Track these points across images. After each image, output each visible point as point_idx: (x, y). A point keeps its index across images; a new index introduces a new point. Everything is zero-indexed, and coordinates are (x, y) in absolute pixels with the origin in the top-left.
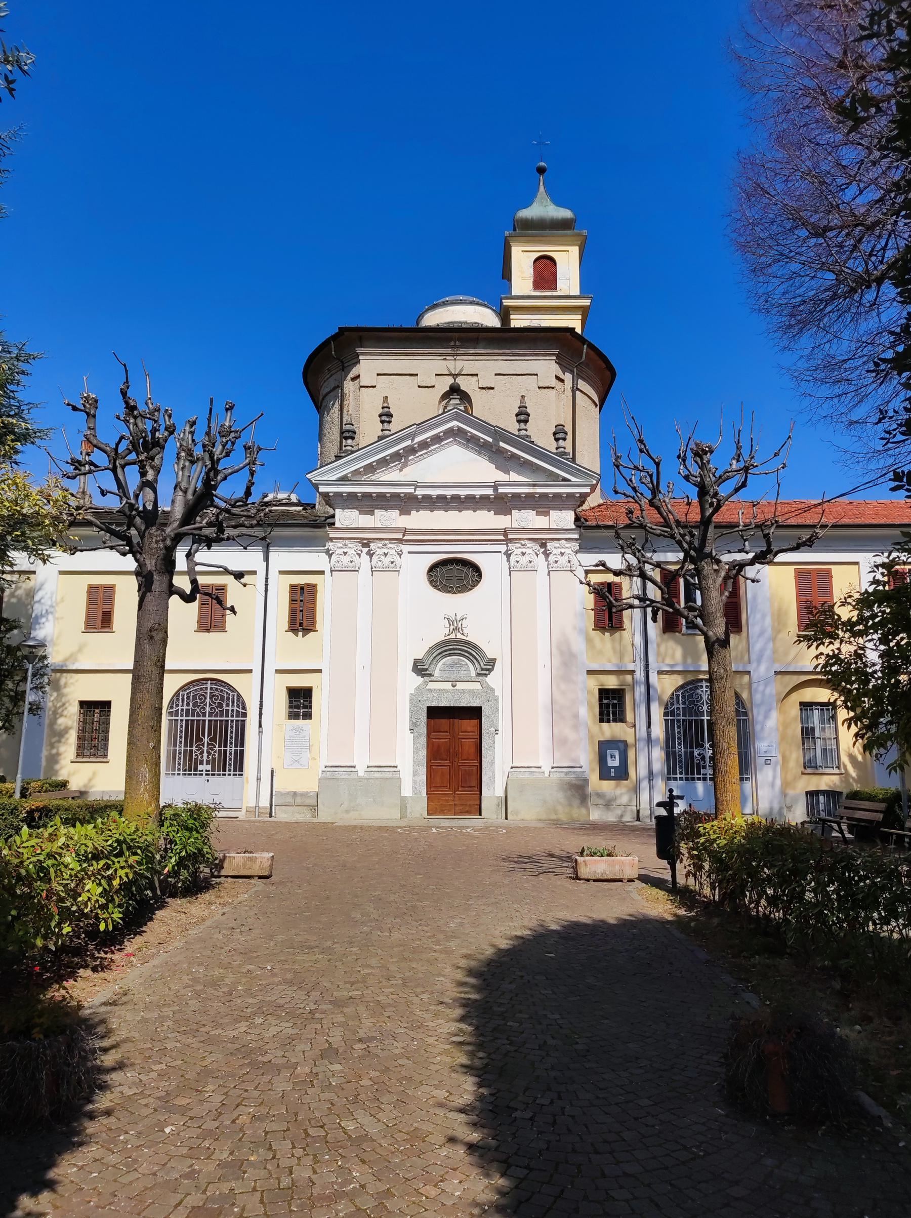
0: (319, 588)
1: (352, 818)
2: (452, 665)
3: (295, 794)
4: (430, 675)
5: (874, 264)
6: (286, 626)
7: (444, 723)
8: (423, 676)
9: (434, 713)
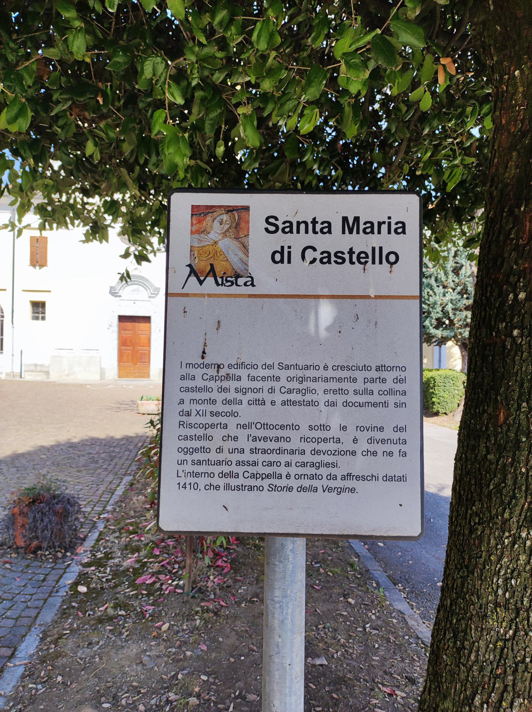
0: (49, 240)
1: (70, 380)
2: (133, 291)
3: (36, 365)
4: (120, 296)
5: (95, 506)
6: (28, 262)
7: (129, 325)
8: (116, 296)
9: (122, 319)
